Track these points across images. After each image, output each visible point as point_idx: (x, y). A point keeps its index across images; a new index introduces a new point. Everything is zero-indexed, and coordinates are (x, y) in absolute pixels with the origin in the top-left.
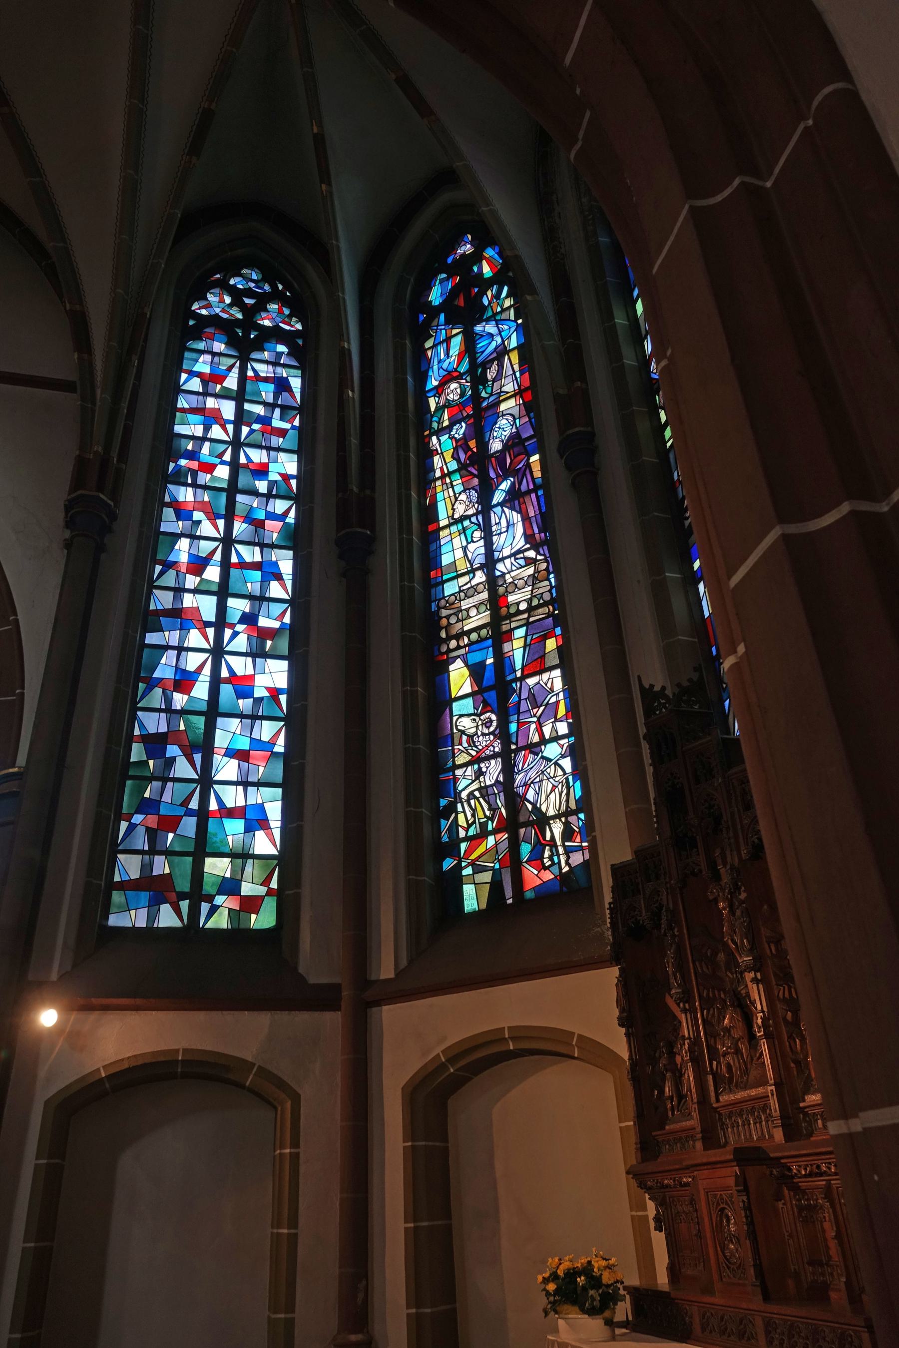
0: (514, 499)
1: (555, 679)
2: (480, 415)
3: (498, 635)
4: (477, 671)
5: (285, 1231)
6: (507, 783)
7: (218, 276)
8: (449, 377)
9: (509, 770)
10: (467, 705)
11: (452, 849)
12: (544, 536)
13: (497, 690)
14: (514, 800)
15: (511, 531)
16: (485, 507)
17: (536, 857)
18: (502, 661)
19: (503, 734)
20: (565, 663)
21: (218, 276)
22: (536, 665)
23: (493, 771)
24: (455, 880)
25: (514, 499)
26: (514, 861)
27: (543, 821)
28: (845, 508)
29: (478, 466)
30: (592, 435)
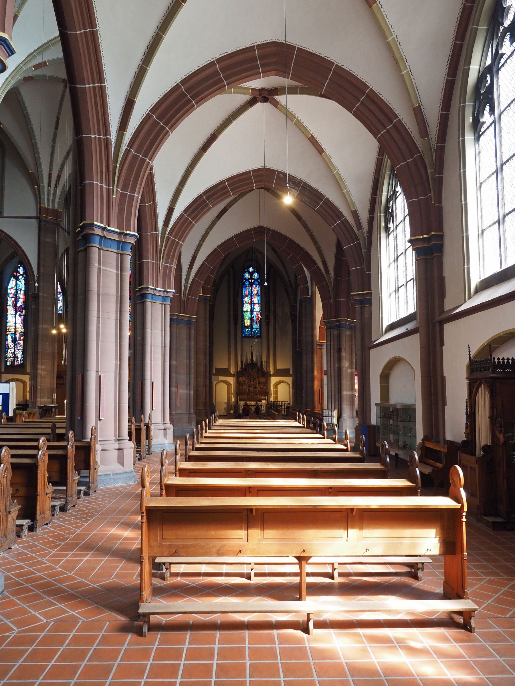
0: (20, 315)
1: (21, 342)
2: (16, 300)
3: (15, 334)
4: (12, 337)
5: (87, 86)
6: (14, 352)
7: (65, 401)
8: (12, 288)
9: (15, 351)
10: (10, 341)
11: (7, 358)
12: (25, 322)
13: (14, 341)
14: (15, 355)
15: (19, 320)
16: (16, 315)
17: (17, 361)
18: (15, 338)
19: (14, 346)
20: (23, 340)
21: (65, 401)
22: (20, 339)
23: (13, 351)
24: (7, 361)
25: (20, 315)
26: (14, 361)
27: (18, 358)
28: (462, 490)
29: (15, 306)
30: (442, 237)
